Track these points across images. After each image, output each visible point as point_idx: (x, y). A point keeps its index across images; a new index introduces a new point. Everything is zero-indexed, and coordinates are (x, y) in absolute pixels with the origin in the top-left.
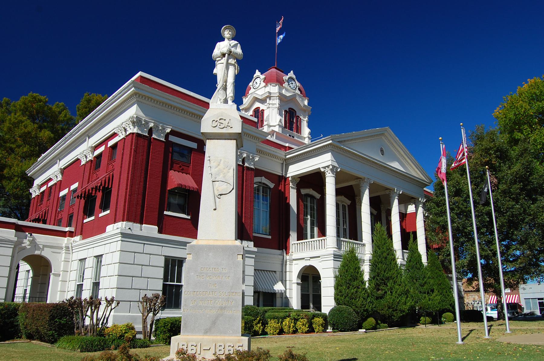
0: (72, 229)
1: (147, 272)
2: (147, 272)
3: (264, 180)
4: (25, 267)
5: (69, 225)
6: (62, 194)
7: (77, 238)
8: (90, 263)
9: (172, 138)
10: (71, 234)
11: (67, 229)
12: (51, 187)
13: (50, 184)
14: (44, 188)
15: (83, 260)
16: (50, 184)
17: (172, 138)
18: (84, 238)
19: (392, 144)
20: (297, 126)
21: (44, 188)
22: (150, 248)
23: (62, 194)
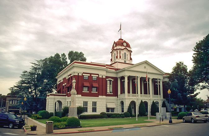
0: (66, 94)
1: (79, 102)
2: (79, 102)
3: (110, 79)
4: (57, 102)
5: (65, 94)
6: (64, 85)
7: (67, 96)
8: (69, 102)
9: (83, 74)
10: (66, 96)
11: (65, 94)
12: (72, 76)
13: (71, 76)
14: (70, 76)
15: (68, 102)
16: (71, 76)
17: (83, 74)
18: (68, 97)
19: (121, 128)
20: (83, 124)
21: (70, 76)
22: (80, 100)
23: (64, 85)
